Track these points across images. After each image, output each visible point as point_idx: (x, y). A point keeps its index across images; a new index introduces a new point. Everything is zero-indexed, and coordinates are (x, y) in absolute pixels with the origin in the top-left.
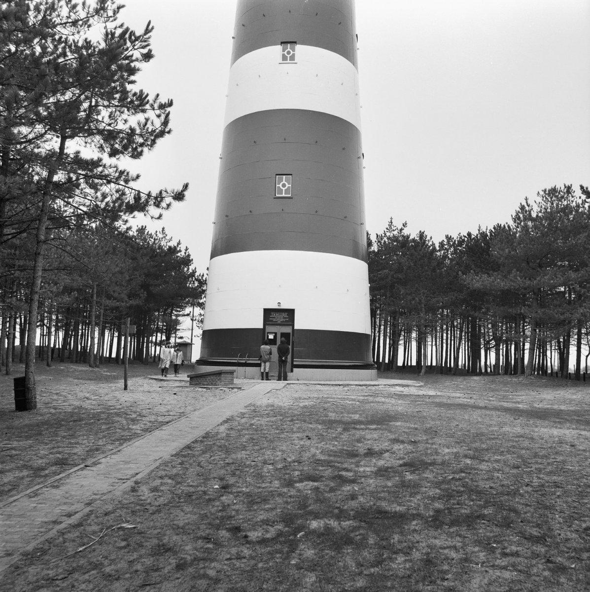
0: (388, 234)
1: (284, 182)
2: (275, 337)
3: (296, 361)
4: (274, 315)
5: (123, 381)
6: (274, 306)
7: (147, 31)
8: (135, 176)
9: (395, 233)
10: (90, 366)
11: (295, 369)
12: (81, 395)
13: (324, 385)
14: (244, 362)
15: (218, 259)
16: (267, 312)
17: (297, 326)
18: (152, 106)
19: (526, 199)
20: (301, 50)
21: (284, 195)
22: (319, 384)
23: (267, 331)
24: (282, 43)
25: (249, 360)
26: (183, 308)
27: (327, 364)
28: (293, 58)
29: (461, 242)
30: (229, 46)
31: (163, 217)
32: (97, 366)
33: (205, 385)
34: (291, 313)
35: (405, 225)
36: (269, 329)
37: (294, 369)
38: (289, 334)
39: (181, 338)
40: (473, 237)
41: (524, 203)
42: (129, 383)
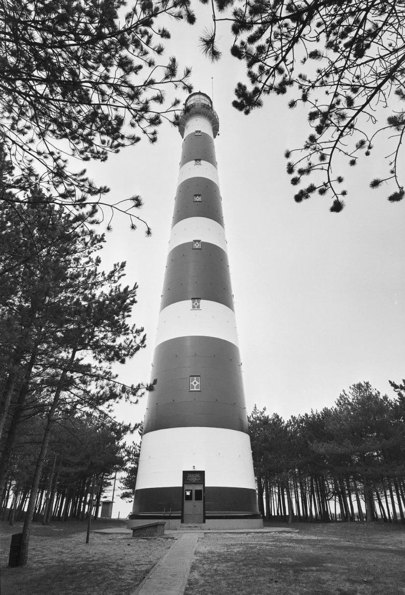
0: (254, 415)
1: (195, 381)
2: (191, 493)
3: (207, 513)
4: (190, 476)
5: (86, 533)
6: (191, 469)
7: (135, 288)
8: (115, 376)
9: (258, 415)
10: (43, 524)
11: (207, 520)
12: (56, 549)
13: (232, 533)
14: (169, 515)
15: (145, 436)
16: (186, 474)
17: (207, 485)
18: (132, 331)
19: (344, 391)
20: (203, 303)
21: (195, 389)
22: (228, 533)
23: (185, 489)
24: (192, 299)
25: (172, 513)
26: (110, 473)
27: (218, 515)
28: (198, 307)
29: (302, 421)
30: (159, 300)
31: (139, 402)
32: (47, 524)
33: (144, 536)
34: (202, 473)
35: (265, 409)
36: (186, 487)
37: (207, 520)
38: (201, 490)
39: (105, 497)
40: (309, 416)
41: (342, 394)
42: (91, 536)
